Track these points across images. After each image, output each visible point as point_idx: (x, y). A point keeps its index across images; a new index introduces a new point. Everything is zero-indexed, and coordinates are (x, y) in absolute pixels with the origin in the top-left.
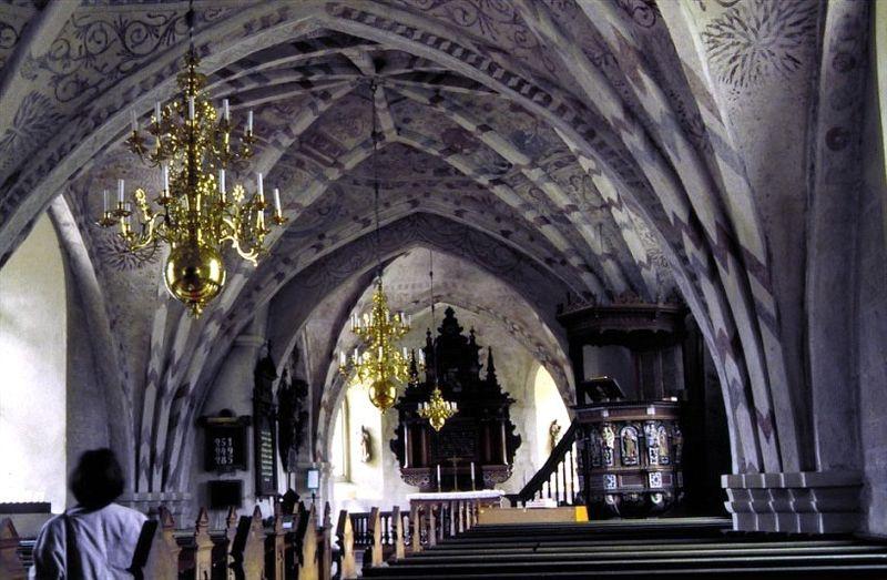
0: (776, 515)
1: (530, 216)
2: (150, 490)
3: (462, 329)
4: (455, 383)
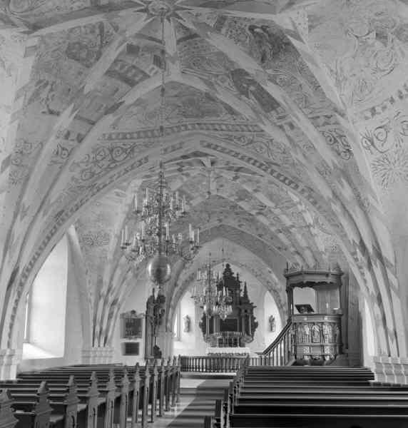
0: (395, 377)
1: (273, 229)
2: (99, 346)
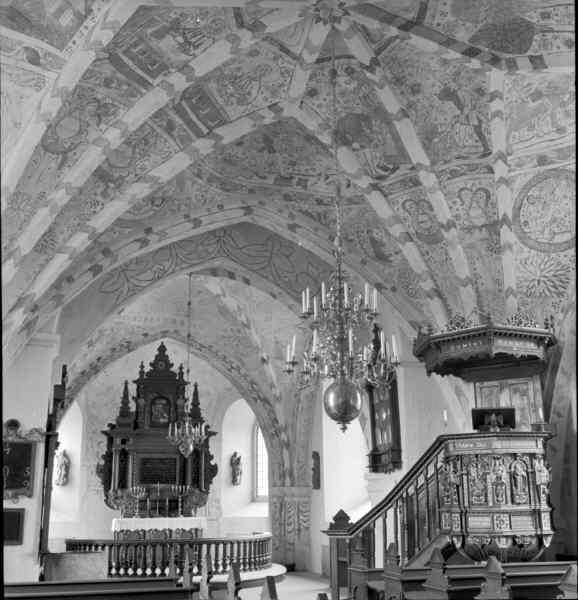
4: (162, 415)
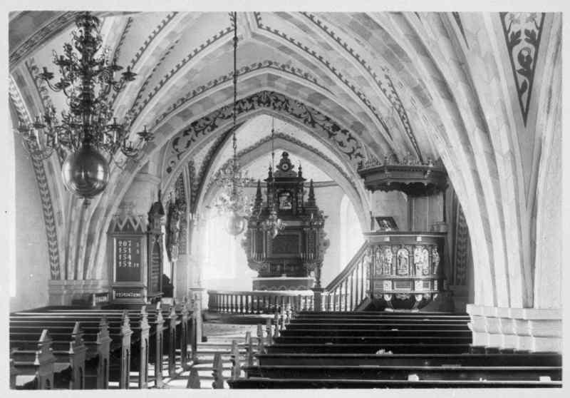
3: (293, 166)
